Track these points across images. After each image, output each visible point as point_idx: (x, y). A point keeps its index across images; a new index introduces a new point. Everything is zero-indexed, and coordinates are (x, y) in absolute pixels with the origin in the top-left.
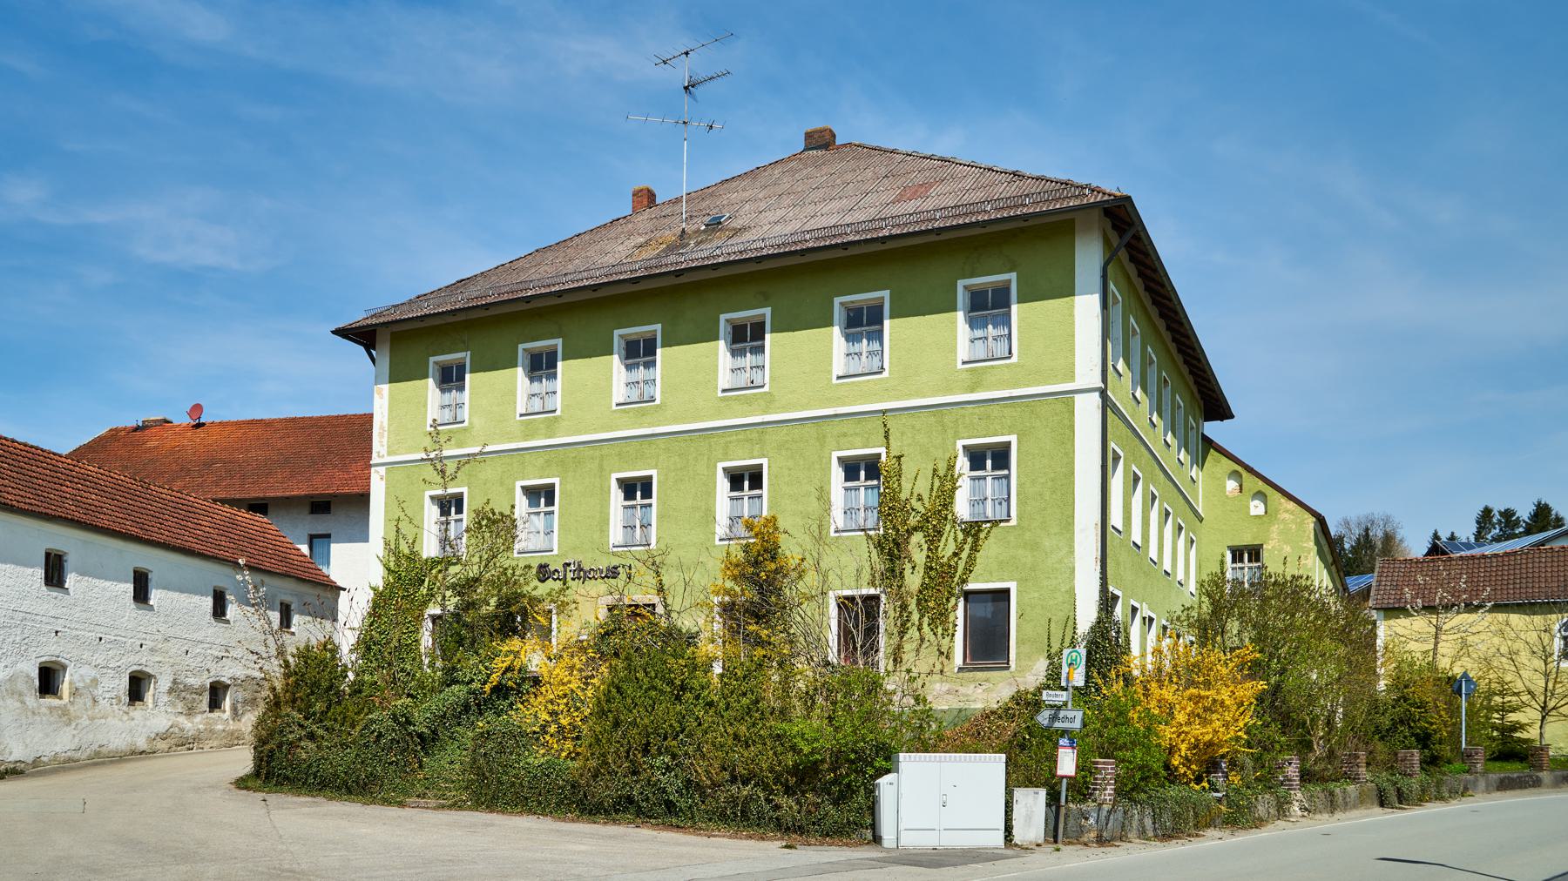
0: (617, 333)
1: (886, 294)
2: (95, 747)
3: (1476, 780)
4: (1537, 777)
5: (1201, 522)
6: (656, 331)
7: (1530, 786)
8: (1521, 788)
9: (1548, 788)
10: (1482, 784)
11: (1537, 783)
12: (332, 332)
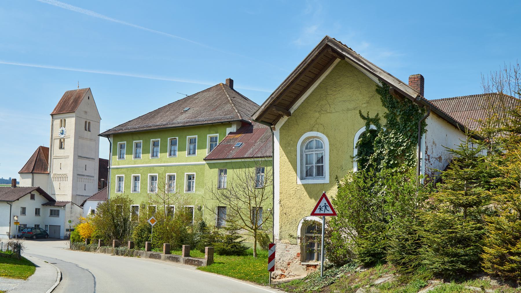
0: (208, 135)
1: (197, 136)
4: (160, 255)
10: (145, 255)
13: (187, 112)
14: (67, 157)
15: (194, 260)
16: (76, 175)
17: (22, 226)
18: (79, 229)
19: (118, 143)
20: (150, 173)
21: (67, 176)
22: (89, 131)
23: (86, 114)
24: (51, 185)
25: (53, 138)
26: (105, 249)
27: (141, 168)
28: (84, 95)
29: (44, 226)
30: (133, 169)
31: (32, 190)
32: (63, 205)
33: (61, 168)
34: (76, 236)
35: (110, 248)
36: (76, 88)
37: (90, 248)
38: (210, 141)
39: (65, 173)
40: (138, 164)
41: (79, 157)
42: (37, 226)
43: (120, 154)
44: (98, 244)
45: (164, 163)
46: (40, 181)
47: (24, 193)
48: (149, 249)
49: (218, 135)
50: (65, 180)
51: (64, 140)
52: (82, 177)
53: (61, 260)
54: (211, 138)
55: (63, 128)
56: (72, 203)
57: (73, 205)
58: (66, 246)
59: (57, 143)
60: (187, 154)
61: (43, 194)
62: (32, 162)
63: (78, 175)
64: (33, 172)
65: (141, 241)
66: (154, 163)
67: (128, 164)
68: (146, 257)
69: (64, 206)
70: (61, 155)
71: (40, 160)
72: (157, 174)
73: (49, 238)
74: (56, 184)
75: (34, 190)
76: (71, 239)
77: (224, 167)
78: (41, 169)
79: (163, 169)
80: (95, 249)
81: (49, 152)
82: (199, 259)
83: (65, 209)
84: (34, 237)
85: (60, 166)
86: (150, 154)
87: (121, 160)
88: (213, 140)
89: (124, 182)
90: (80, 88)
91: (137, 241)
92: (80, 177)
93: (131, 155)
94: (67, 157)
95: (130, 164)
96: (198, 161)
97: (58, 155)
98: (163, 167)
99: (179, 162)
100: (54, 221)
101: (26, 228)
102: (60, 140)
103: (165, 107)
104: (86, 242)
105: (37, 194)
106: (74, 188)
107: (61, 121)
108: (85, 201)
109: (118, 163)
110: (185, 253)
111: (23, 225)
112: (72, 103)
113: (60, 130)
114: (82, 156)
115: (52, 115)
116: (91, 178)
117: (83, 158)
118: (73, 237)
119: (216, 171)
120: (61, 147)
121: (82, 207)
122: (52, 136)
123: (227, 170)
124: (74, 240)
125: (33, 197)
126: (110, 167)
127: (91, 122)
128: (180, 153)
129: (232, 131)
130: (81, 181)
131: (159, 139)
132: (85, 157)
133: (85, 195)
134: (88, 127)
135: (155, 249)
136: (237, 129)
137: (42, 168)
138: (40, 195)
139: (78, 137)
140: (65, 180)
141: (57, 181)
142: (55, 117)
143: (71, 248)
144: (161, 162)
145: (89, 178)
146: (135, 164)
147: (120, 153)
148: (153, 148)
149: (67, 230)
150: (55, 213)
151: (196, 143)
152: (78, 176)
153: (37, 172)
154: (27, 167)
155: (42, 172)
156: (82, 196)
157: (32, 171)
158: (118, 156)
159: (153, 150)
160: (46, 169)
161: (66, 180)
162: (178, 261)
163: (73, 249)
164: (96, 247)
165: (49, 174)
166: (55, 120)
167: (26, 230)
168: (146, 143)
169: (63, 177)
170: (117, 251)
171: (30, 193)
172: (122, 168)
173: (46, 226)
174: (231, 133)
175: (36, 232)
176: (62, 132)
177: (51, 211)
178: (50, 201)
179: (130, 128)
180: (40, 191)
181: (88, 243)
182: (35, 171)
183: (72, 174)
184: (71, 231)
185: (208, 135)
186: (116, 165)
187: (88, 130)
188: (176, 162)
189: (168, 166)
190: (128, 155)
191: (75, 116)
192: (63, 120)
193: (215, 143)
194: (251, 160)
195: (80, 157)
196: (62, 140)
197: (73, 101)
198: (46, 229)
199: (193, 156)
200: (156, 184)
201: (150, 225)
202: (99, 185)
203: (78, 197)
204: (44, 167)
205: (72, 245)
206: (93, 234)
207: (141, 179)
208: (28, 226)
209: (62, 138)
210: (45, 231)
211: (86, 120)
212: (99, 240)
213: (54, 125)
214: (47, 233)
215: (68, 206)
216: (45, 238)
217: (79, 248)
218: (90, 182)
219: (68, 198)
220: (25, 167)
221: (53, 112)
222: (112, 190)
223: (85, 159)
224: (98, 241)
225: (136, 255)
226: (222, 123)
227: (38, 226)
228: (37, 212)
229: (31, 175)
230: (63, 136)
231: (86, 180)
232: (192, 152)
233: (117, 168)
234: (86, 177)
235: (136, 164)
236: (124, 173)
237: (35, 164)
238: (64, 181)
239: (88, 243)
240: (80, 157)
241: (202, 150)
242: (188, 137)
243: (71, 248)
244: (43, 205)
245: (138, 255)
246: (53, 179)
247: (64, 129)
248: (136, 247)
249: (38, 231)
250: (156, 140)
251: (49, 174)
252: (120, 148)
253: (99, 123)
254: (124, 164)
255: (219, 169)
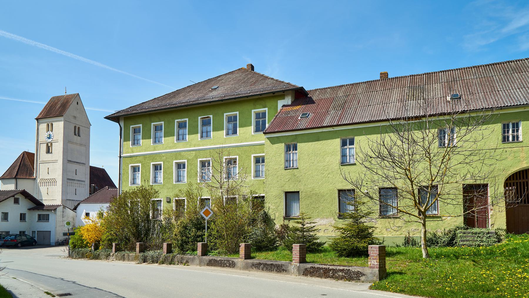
0: (253, 111)
1: (238, 113)
2: (57, 239)
3: (194, 259)
4: (233, 262)
5: (356, 165)
6: (237, 114)
7: (227, 266)
8: (221, 266)
9: (240, 269)
10: (197, 261)
11: (232, 265)
12: (104, 118)
13: (217, 90)
14: (55, 161)
15: (333, 269)
16: (66, 179)
17: (4, 233)
18: (82, 232)
19: (131, 126)
20: (176, 159)
21: (55, 180)
22: (79, 136)
23: (75, 119)
24: (37, 191)
25: (39, 143)
26: (124, 255)
27: (163, 155)
28: (73, 100)
29: (31, 232)
30: (152, 157)
31: (15, 193)
32: (54, 208)
33: (48, 173)
34: (77, 241)
35: (132, 254)
36: (64, 94)
37: (99, 255)
38: (255, 118)
39: (54, 178)
40: (159, 150)
41: (68, 161)
42: (22, 233)
43: (134, 140)
44: (112, 249)
45: (195, 146)
46: (25, 185)
47: (6, 197)
48: (205, 253)
49: (266, 109)
50: (53, 185)
51: (52, 144)
52: (72, 181)
53: (74, 282)
54: (258, 115)
55: (50, 132)
56: (64, 207)
57: (65, 208)
58: (62, 254)
59: (44, 148)
60: (225, 134)
61: (29, 198)
62: (15, 167)
63: (68, 179)
64: (17, 177)
65: (187, 243)
66: (181, 147)
67: (145, 151)
68: (204, 265)
69: (55, 210)
70: (49, 160)
71: (25, 165)
72: (186, 161)
73: (38, 245)
74: (43, 190)
75: (18, 193)
76: (71, 246)
77: (293, 141)
78: (26, 175)
79: (194, 154)
80: (107, 257)
81: (34, 157)
82: (350, 268)
83: (55, 213)
84: (19, 245)
85: (47, 171)
86: (175, 137)
87: (135, 147)
88: (261, 116)
89: (140, 172)
90: (68, 94)
91: (180, 242)
92: (70, 181)
93: (150, 140)
94: (55, 161)
95: (148, 151)
96: (241, 142)
97: (45, 160)
98: (194, 152)
99: (215, 145)
100: (43, 226)
101: (9, 235)
102: (47, 144)
103: (184, 89)
104: (93, 248)
105: (21, 198)
106: (64, 192)
107: (48, 125)
108: (79, 204)
109: (132, 150)
110: (167, 250)
111: (5, 232)
112: (59, 108)
113: (47, 134)
114: (71, 160)
115: (37, 119)
116: (82, 183)
117: (73, 163)
118: (73, 243)
119: (281, 146)
120: (48, 151)
121: (75, 211)
122: (38, 140)
123: (298, 144)
124: (74, 247)
125: (16, 201)
126: (121, 156)
127: (81, 128)
128: (216, 133)
129: (286, 104)
130: (71, 185)
131: (187, 119)
132: (75, 162)
133: (75, 200)
134: (77, 132)
135: (212, 252)
136: (292, 101)
137: (27, 173)
138: (25, 198)
139: (67, 141)
140: (53, 185)
141: (44, 186)
142: (40, 121)
143: (70, 256)
144: (190, 146)
145: (80, 182)
146: (155, 150)
147: (133, 139)
148: (178, 130)
149: (65, 234)
150: (44, 218)
151: (236, 121)
152: (68, 180)
153: (20, 177)
154: (10, 173)
155: (27, 178)
156: (73, 200)
157: (15, 177)
158: (131, 142)
159: (178, 133)
160: (32, 174)
161: (55, 184)
162: (283, 270)
163: (74, 257)
164: (110, 254)
165: (35, 179)
166: (41, 125)
167: (9, 238)
168: (170, 125)
169: (53, 182)
170: (145, 258)
171: (13, 196)
172: (137, 156)
173: (34, 232)
174: (284, 106)
175: (21, 240)
176: (49, 136)
177: (39, 215)
178: (38, 205)
179: (146, 108)
180: (24, 193)
181: (97, 248)
182: (19, 177)
183: (62, 178)
184: (69, 235)
185: (253, 111)
186: (128, 153)
187: (77, 135)
188: (211, 145)
189: (199, 150)
190: (144, 140)
191: (63, 120)
192: (50, 124)
193: (263, 119)
194: (333, 130)
195: (70, 161)
196: (49, 145)
197: (61, 106)
198: (34, 235)
199: (234, 136)
200: (185, 173)
201: (202, 218)
202: (90, 191)
203: (68, 201)
204: (29, 173)
205: (72, 252)
206: (104, 237)
207: (163, 168)
208: (11, 233)
209: (49, 142)
210: (32, 238)
211: (75, 125)
212: (114, 244)
213: (39, 129)
214: (34, 239)
215: (59, 209)
216: (32, 245)
217: (83, 256)
218: (80, 186)
219: (58, 201)
220: (7, 173)
221: (38, 117)
222: (124, 183)
223: (75, 163)
224: (112, 246)
225: (181, 262)
226: (274, 93)
227: (24, 232)
228: (23, 217)
229: (14, 181)
230: (50, 140)
231: (77, 184)
232: (230, 132)
233: (131, 157)
234: (76, 182)
235: (156, 150)
236: (140, 162)
237: (18, 170)
238: (52, 185)
239: (97, 248)
240: (70, 161)
241: (245, 129)
242: (225, 114)
243: (70, 256)
244: (29, 209)
245: (185, 261)
246: (40, 184)
247: (51, 133)
248: (176, 251)
249: (24, 238)
250: (183, 120)
251: (35, 179)
252: (133, 133)
253: (89, 128)
254: (140, 151)
255: (285, 144)
